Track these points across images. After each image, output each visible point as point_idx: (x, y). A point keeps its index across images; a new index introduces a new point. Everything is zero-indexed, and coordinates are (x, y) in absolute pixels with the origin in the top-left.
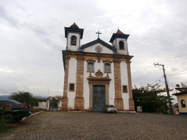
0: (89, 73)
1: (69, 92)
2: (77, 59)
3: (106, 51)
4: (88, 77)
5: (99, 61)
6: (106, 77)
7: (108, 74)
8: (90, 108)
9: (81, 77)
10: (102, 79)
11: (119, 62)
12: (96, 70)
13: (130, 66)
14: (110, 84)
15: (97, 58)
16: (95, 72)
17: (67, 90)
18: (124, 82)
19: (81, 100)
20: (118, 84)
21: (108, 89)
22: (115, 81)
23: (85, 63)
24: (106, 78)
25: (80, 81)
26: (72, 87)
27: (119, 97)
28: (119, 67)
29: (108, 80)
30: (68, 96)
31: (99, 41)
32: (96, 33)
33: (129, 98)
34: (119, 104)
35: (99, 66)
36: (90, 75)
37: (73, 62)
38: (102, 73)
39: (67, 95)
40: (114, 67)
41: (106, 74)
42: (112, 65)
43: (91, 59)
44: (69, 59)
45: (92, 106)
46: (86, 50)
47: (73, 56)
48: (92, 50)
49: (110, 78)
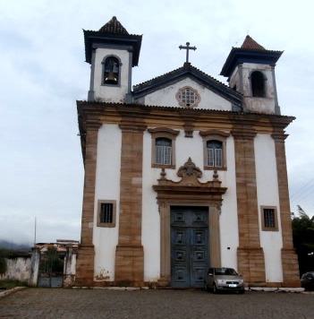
0: (160, 170)
1: (100, 229)
2: (121, 128)
3: (209, 101)
4: (157, 183)
5: (189, 134)
6: (212, 182)
7: (215, 172)
9: (135, 181)
10: (198, 188)
12: (180, 162)
14: (223, 202)
15: (183, 124)
16: (178, 167)
18: (267, 196)
20: (247, 203)
21: (218, 219)
23: (148, 140)
24: (210, 185)
26: (107, 213)
27: (252, 244)
28: (252, 151)
29: (216, 192)
30: (95, 242)
31: (188, 71)
32: (181, 47)
35: (189, 149)
36: (163, 174)
37: (110, 138)
38: (198, 170)
39: (92, 238)
42: (230, 144)
44: (98, 128)
45: (168, 272)
46: (151, 100)
48: (167, 98)
49: (223, 186)
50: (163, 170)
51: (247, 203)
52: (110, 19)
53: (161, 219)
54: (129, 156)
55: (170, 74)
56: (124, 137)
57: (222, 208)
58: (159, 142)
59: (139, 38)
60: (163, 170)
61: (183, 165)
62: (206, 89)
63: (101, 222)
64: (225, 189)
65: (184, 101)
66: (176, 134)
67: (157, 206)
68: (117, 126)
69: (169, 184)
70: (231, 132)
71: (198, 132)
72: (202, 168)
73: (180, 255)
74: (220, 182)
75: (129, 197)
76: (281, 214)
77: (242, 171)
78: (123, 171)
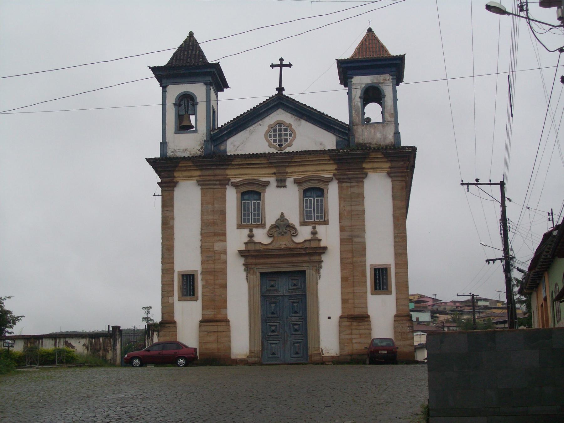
0: (246, 232)
1: (181, 303)
2: (199, 185)
3: (308, 138)
4: (243, 248)
5: (281, 184)
6: (310, 240)
7: (314, 228)
8: (251, 352)
9: (218, 246)
10: (290, 249)
11: (360, 179)
12: (271, 219)
13: (172, 198)
14: (323, 264)
15: (274, 170)
16: (268, 226)
17: (173, 295)
18: (378, 251)
19: (221, 328)
20: (352, 263)
21: (317, 283)
22: (342, 252)
23: (232, 196)
24: (307, 245)
25: (214, 263)
26: (188, 284)
27: (357, 312)
28: (361, 196)
29: (315, 252)
30: (178, 317)
31: (280, 101)
32: (273, 66)
33: (394, 312)
34: (354, 336)
35: (282, 202)
36: (251, 236)
37: (189, 195)
38: (293, 227)
39: (173, 313)
40: (340, 198)
41: (309, 229)
42: (333, 191)
43: (250, 177)
44: (175, 186)
45: (258, 348)
46: (235, 145)
47: (185, 174)
48: (254, 142)
49: (322, 244)
50: (251, 231)
51: (352, 263)
52: (185, 36)
53: (250, 288)
54: (210, 217)
55: (207, 110)
56: (203, 195)
57: (322, 271)
58: (246, 197)
59: (401, 59)
60: (251, 231)
61: (274, 223)
62: (303, 122)
63: (183, 295)
64: (325, 248)
65: (275, 141)
66: (266, 184)
67: (244, 274)
68: (194, 182)
69: (258, 247)
70: (334, 175)
71: (292, 179)
72: (297, 225)
73: (273, 328)
74: (320, 240)
75: (212, 266)
76: (396, 273)
77: (347, 223)
78: (204, 235)
